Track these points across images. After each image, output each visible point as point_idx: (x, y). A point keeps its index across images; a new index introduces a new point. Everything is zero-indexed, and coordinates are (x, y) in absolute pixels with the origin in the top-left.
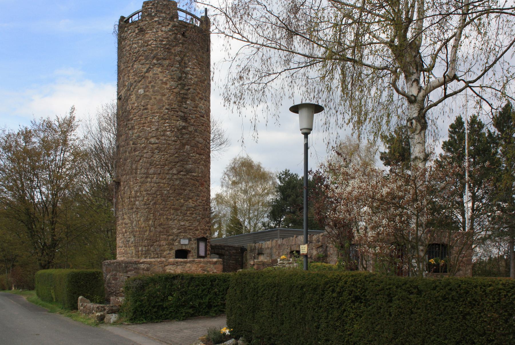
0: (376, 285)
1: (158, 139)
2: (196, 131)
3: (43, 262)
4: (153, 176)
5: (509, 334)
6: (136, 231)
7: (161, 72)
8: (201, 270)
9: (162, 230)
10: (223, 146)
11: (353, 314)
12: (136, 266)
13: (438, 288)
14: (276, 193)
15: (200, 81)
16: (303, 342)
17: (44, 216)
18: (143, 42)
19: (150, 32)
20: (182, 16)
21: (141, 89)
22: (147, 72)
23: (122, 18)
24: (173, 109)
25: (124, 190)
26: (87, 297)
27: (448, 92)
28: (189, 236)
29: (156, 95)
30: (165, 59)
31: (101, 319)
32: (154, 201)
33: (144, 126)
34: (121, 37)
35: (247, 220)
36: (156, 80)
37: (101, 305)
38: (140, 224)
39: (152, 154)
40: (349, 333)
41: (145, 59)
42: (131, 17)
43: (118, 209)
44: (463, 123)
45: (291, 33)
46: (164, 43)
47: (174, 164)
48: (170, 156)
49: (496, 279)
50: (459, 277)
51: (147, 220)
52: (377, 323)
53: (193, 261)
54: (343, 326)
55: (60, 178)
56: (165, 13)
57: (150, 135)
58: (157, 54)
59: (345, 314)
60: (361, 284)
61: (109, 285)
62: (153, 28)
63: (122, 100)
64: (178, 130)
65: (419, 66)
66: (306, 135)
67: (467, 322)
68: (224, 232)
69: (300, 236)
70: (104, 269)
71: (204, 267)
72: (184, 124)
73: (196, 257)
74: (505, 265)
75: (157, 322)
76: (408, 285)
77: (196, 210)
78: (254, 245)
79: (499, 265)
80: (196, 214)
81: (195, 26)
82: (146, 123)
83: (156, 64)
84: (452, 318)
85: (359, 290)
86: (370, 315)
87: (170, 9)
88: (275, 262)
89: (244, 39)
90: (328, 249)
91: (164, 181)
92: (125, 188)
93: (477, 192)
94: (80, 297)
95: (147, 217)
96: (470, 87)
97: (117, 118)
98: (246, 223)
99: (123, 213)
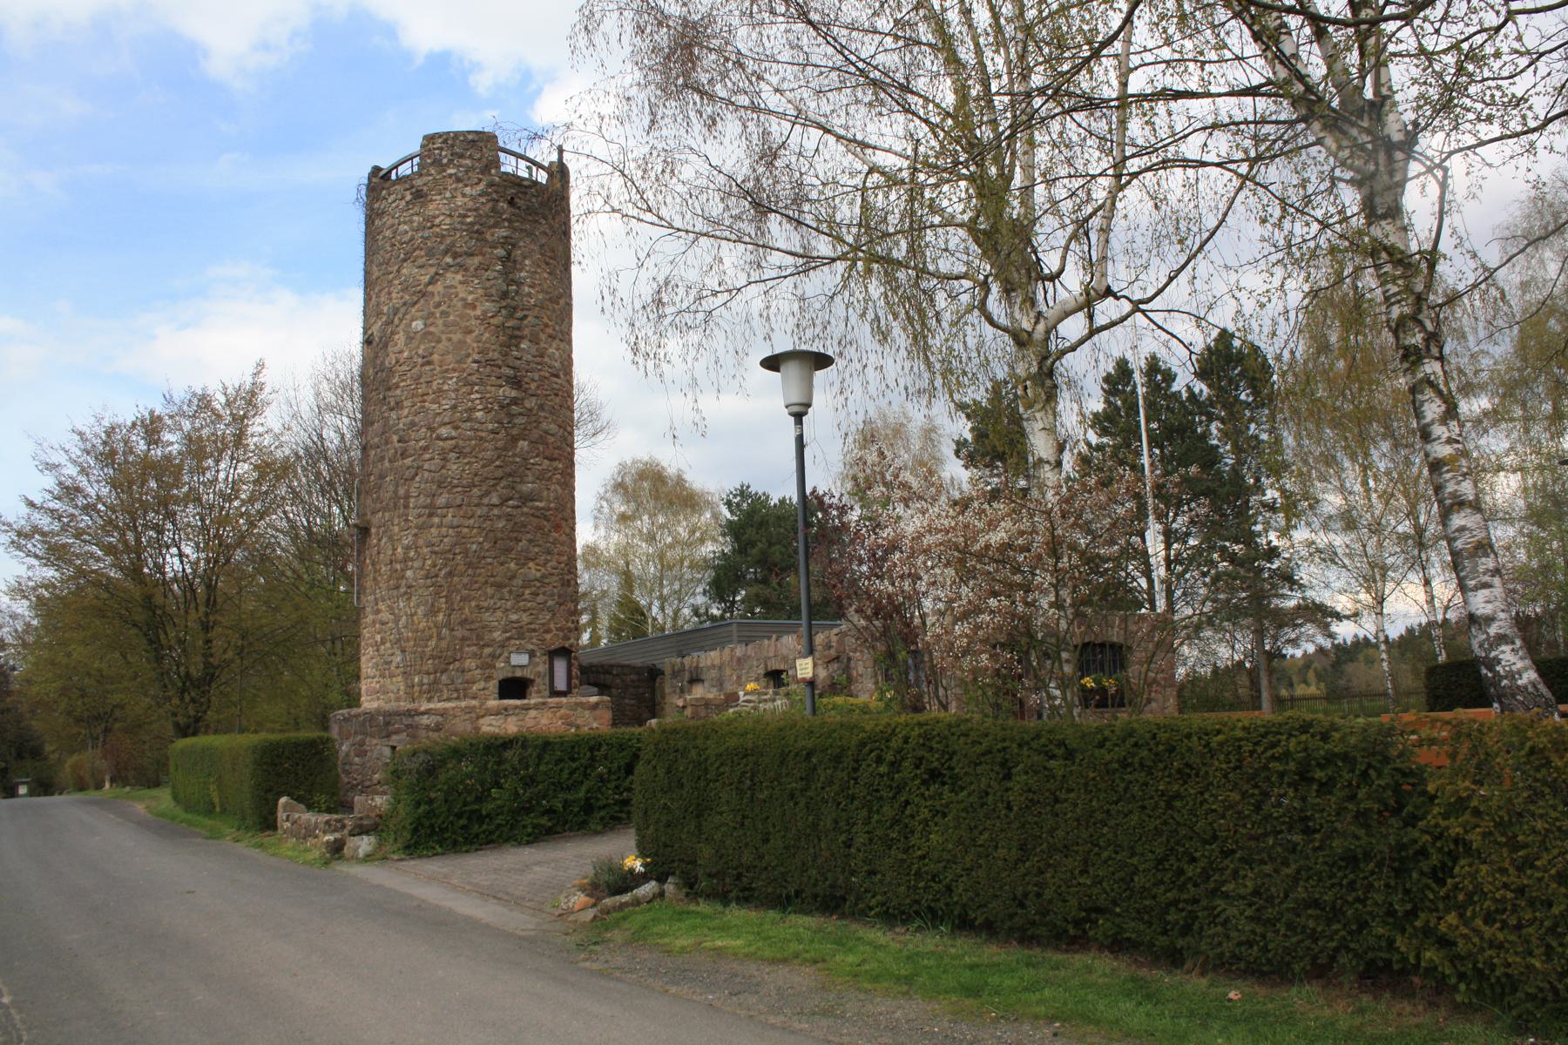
0: (974, 743)
1: (456, 428)
2: (541, 407)
3: (182, 720)
4: (445, 511)
5: (1265, 835)
6: (408, 640)
7: (461, 283)
9: (467, 633)
10: (600, 437)
11: (926, 811)
12: (409, 721)
13: (1108, 744)
14: (720, 539)
15: (550, 300)
16: (816, 880)
17: (186, 612)
20: (509, 165)
22: (430, 283)
23: (376, 170)
24: (490, 363)
25: (378, 545)
26: (299, 799)
27: (1100, 320)
28: (530, 647)
29: (450, 332)
30: (472, 255)
31: (337, 849)
32: (448, 569)
33: (424, 401)
34: (372, 210)
35: (656, 603)
36: (451, 300)
37: (335, 816)
39: (442, 463)
40: (919, 853)
42: (396, 167)
43: (365, 588)
44: (1132, 372)
45: (762, 209)
46: (469, 220)
48: (484, 466)
49: (1229, 717)
50: (1149, 716)
51: (432, 611)
52: (981, 828)
53: (544, 704)
54: (906, 838)
55: (223, 521)
56: (471, 157)
58: (453, 244)
59: (908, 812)
60: (940, 742)
61: (347, 767)
62: (446, 189)
63: (374, 344)
64: (502, 407)
65: (1035, 272)
66: (799, 417)
67: (1175, 815)
68: (603, 633)
69: (785, 637)
70: (334, 733)
71: (568, 716)
72: (514, 394)
73: (547, 693)
74: (1248, 683)
75: (467, 851)
76: (1043, 740)
77: (544, 585)
78: (679, 660)
79: (1235, 684)
80: (544, 594)
81: (536, 183)
84: (1144, 808)
85: (937, 756)
86: (965, 810)
88: (732, 698)
89: (664, 223)
90: (852, 664)
91: (472, 521)
92: (380, 540)
93: (1174, 521)
94: (283, 800)
95: (433, 605)
96: (1143, 312)
97: (364, 384)
98: (655, 610)
99: (376, 599)
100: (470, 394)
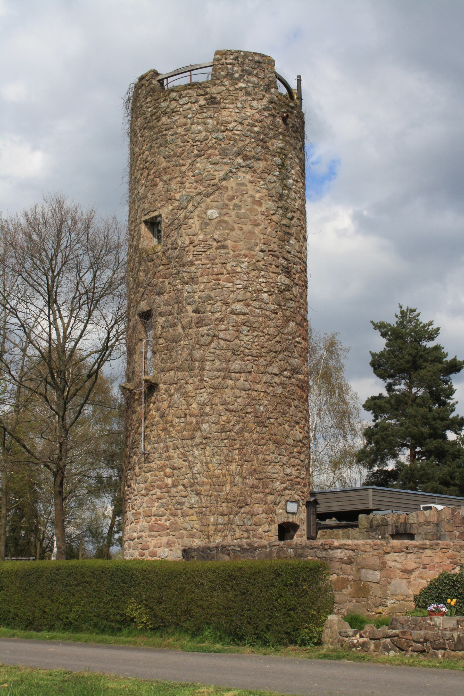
1: (248, 305)
6: (203, 484)
8: (451, 563)
18: (215, 123)
19: (231, 106)
21: (212, 208)
22: (225, 179)
30: (259, 159)
32: (241, 425)
36: (243, 196)
38: (212, 469)
41: (220, 154)
46: (256, 129)
47: (274, 355)
48: (268, 340)
56: (257, 75)
57: (231, 296)
62: (237, 100)
72: (287, 281)
82: (222, 274)
83: (243, 167)
87: (264, 71)
100: (258, 278)
